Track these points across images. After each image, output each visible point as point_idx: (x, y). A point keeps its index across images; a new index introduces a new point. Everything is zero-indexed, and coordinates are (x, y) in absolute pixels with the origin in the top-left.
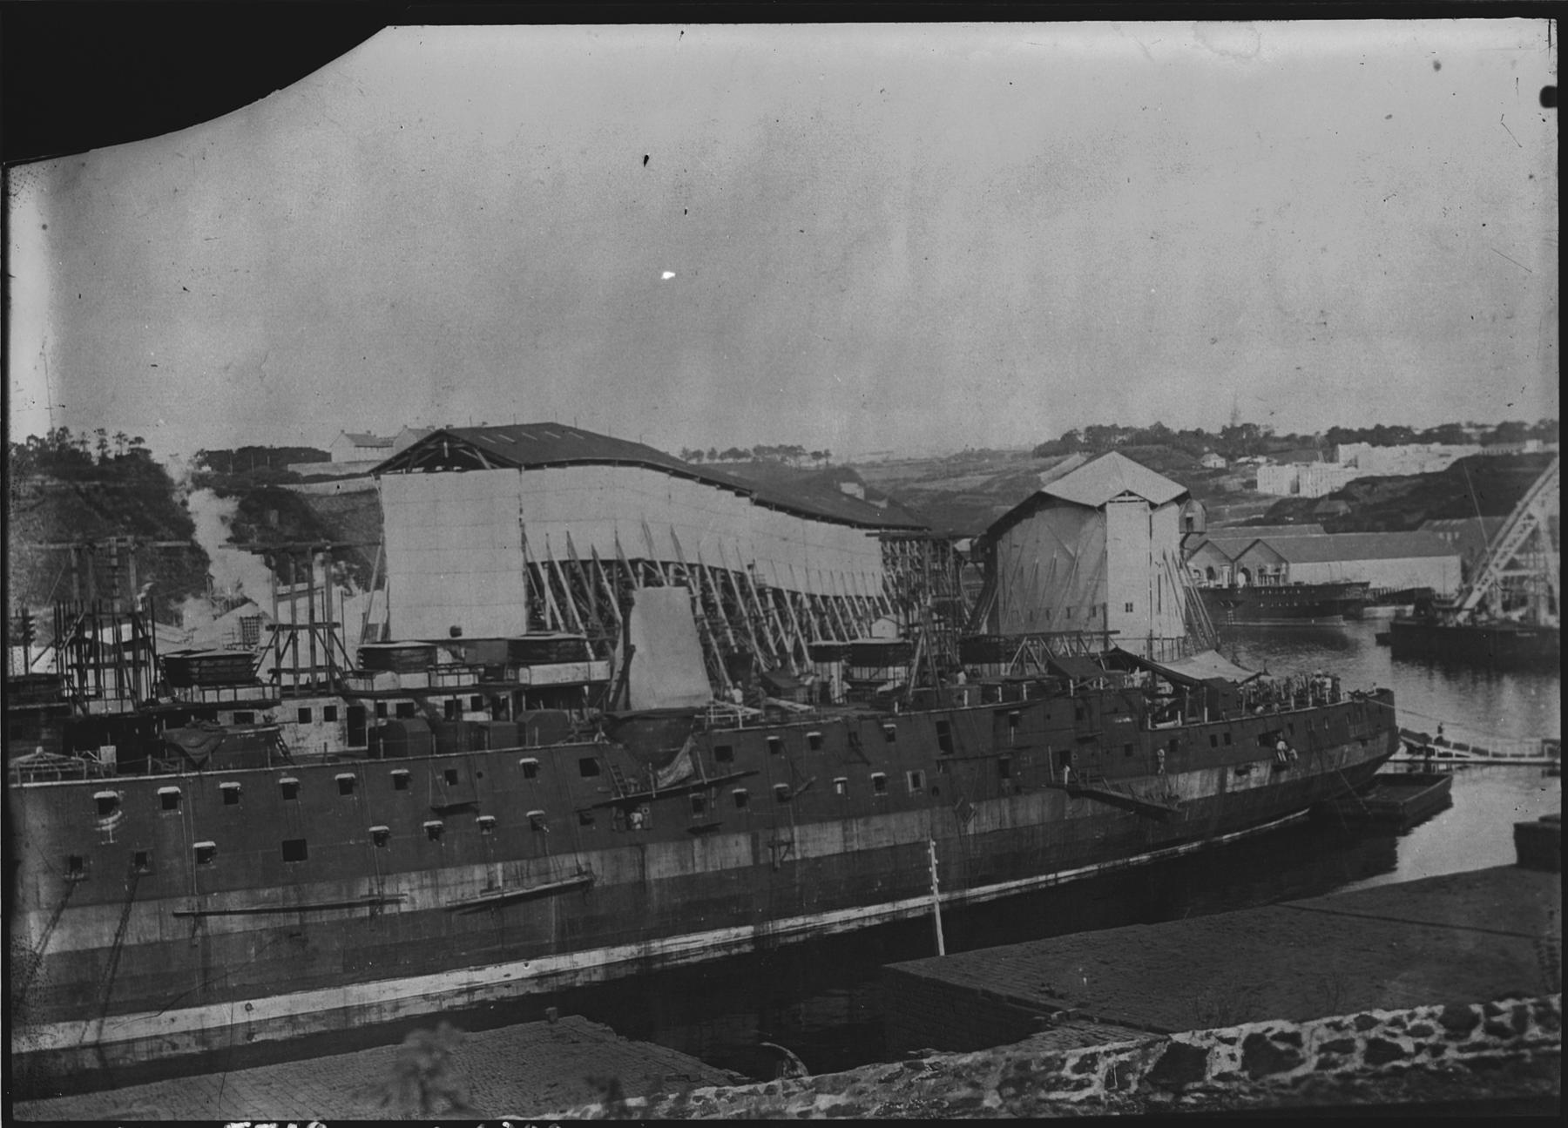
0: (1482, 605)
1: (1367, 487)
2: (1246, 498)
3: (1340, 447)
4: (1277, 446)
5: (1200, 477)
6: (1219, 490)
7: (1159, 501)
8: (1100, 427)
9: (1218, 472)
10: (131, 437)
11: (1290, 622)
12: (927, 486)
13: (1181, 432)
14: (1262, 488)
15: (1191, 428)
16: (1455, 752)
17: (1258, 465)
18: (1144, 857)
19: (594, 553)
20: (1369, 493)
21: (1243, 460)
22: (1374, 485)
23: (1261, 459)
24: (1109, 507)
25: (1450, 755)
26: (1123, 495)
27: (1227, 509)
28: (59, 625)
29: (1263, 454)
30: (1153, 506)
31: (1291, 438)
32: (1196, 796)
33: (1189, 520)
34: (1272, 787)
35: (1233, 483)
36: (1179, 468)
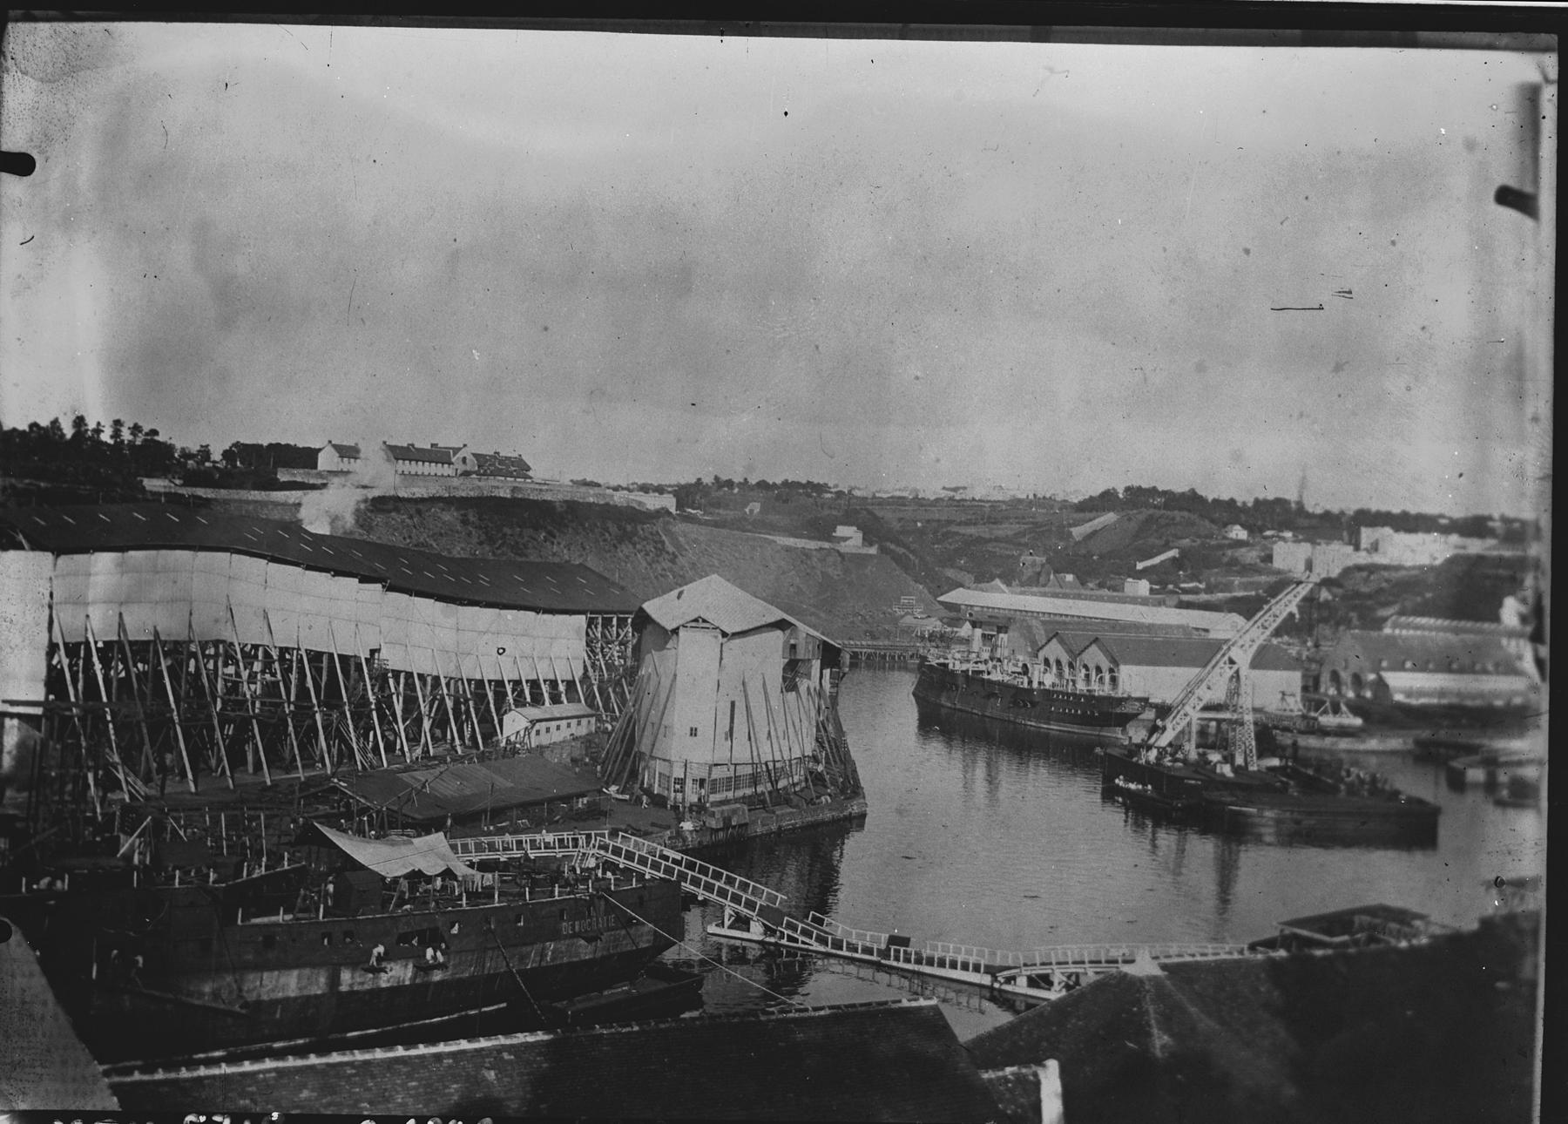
0: (1175, 746)
1: (1365, 574)
2: (1259, 572)
3: (1363, 530)
4: (1306, 523)
5: (1220, 547)
6: (1234, 562)
7: (729, 631)
8: (1140, 488)
9: (1239, 544)
10: (146, 429)
11: (1076, 729)
12: (962, 530)
13: (1215, 501)
14: (1278, 563)
15: (1225, 497)
16: (801, 938)
17: (1284, 539)
18: (301, 1041)
19: (156, 634)
20: (1366, 580)
21: (1268, 533)
22: (1371, 573)
23: (1288, 534)
24: (682, 632)
25: (796, 941)
26: (696, 620)
27: (1237, 581)
28: (536, 529)
29: (1289, 528)
30: (724, 634)
31: (1327, 515)
32: (292, 995)
33: (793, 647)
34: (413, 987)
35: (1251, 556)
36: (1199, 537)
